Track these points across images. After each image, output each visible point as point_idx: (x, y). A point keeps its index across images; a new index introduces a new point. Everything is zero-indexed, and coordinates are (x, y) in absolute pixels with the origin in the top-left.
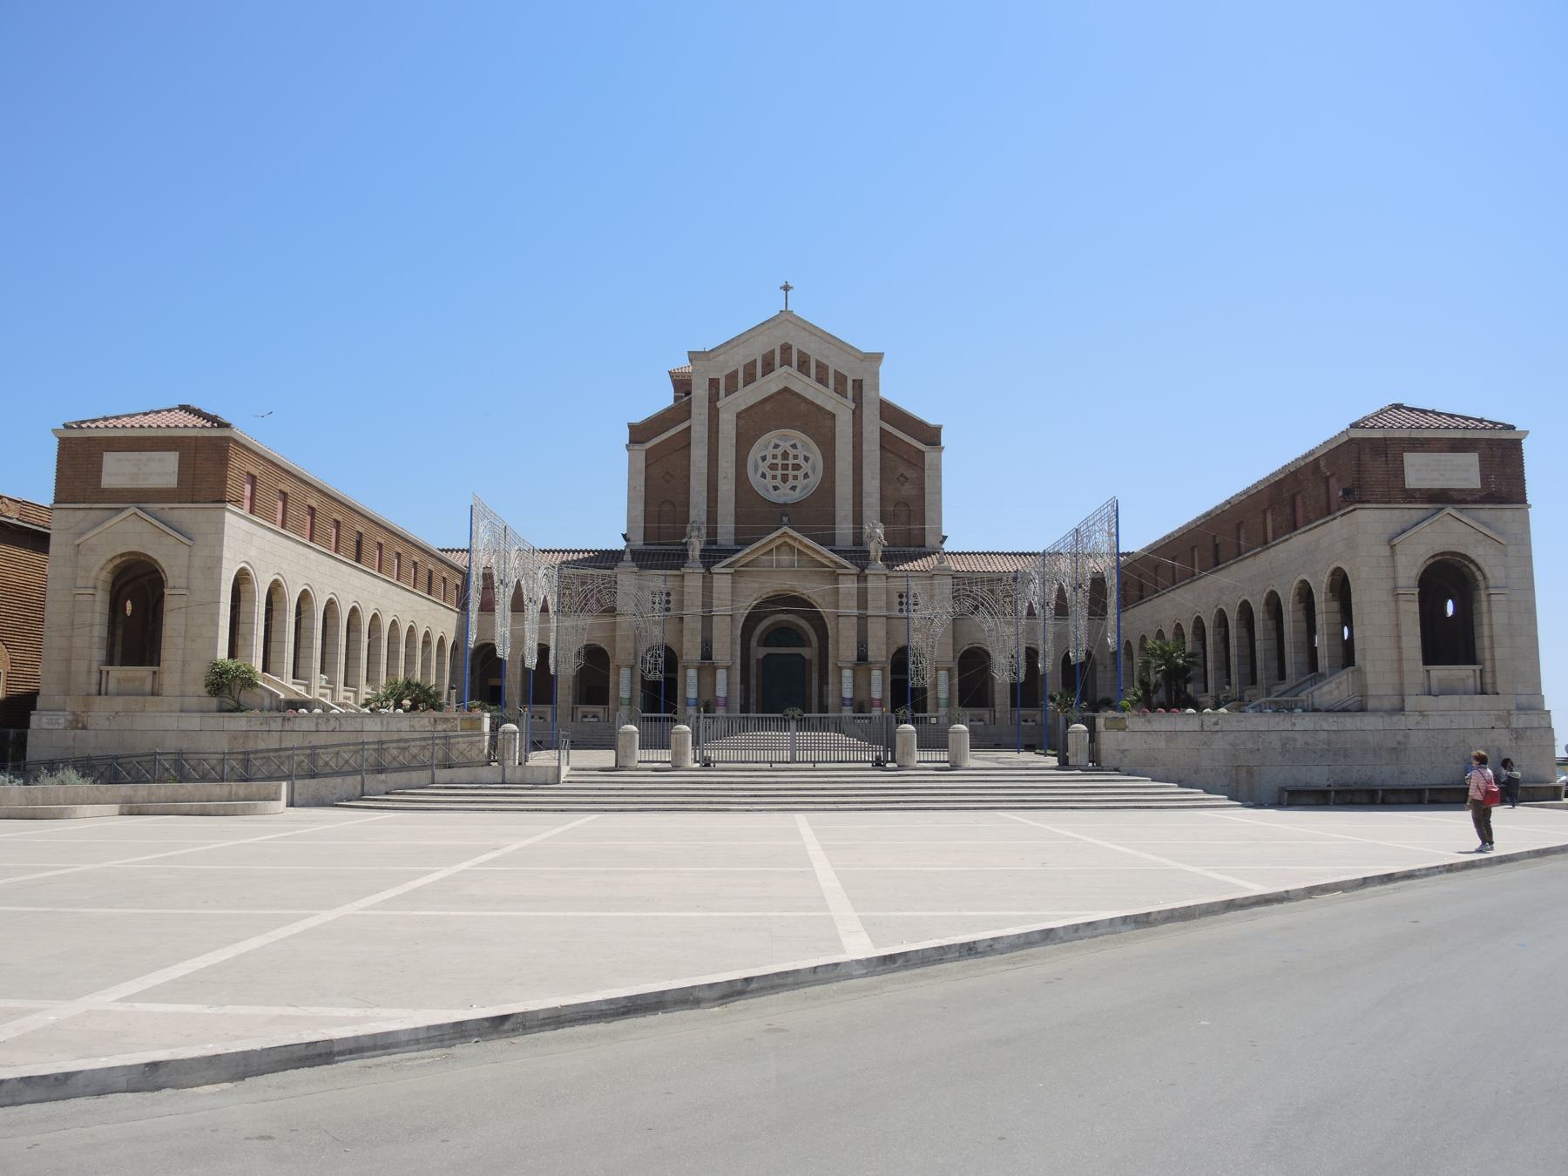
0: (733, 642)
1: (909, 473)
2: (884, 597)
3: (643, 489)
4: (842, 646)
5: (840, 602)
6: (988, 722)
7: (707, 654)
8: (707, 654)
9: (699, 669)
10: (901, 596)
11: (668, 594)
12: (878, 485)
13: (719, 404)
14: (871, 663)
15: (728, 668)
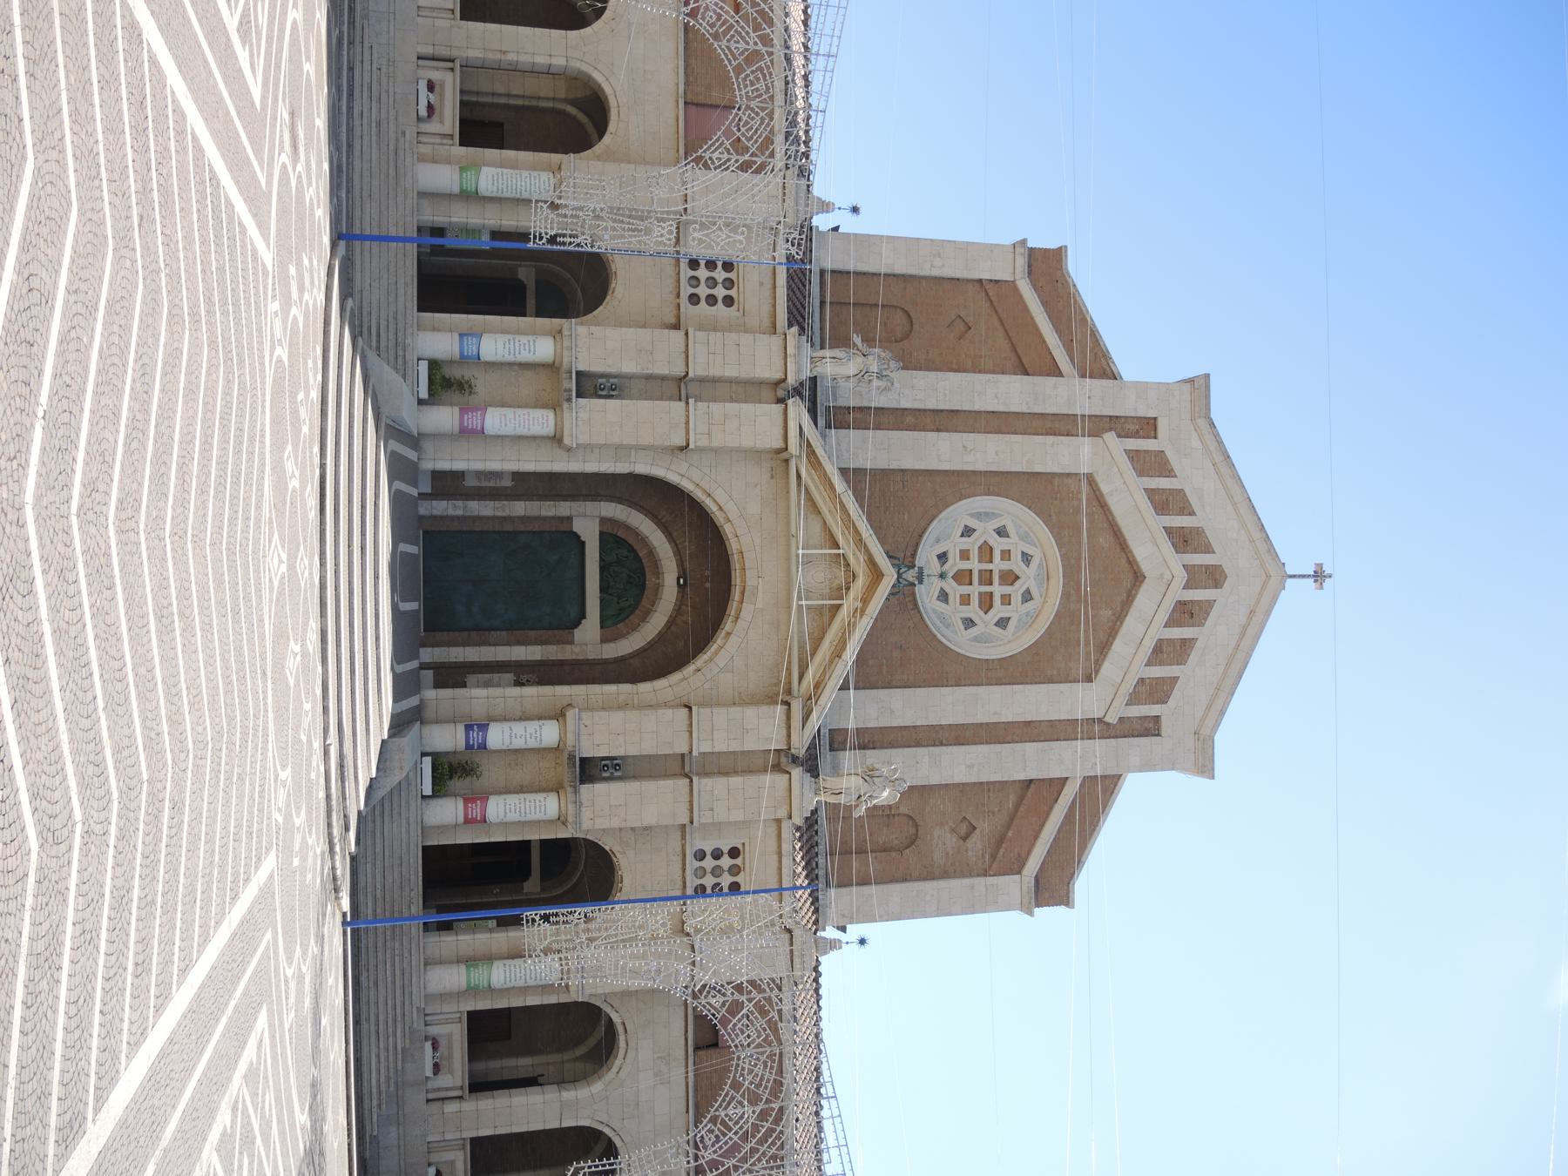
0: (620, 450)
1: (976, 843)
2: (738, 816)
3: (936, 272)
4: (617, 718)
5: (723, 710)
6: (431, 1085)
7: (591, 385)
8: (591, 385)
9: (551, 368)
10: (734, 853)
11: (729, 301)
12: (957, 780)
13: (1110, 437)
14: (576, 792)
15: (556, 439)
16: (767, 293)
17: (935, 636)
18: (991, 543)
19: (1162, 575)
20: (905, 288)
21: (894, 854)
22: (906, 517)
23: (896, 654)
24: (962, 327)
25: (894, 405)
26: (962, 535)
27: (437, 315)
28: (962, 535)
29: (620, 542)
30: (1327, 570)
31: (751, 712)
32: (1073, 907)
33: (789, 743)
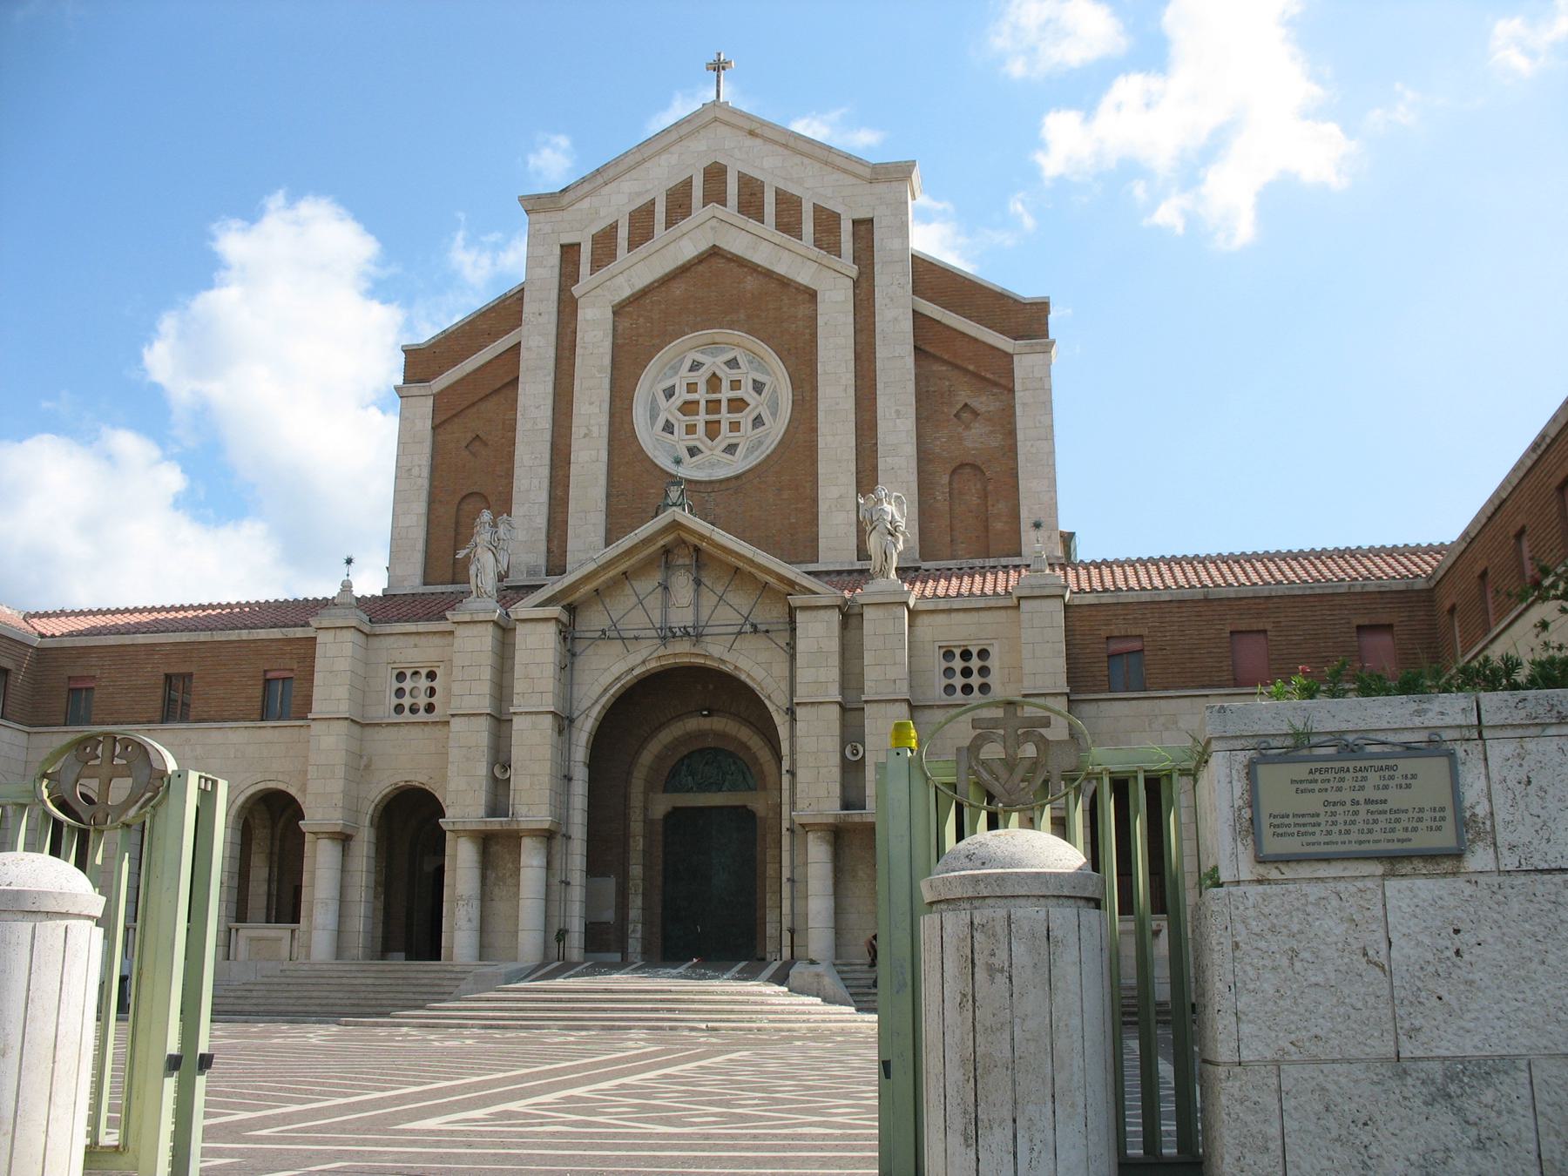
1: (984, 403)
3: (425, 472)
16: (422, 641)
17: (768, 456)
18: (679, 403)
19: (712, 228)
20: (440, 501)
21: (990, 488)
22: (652, 491)
23: (785, 495)
24: (477, 443)
25: (545, 509)
26: (672, 433)
27: (443, 945)
28: (672, 433)
29: (674, 772)
30: (712, 58)
31: (801, 645)
32: (1049, 298)
33: (832, 607)
